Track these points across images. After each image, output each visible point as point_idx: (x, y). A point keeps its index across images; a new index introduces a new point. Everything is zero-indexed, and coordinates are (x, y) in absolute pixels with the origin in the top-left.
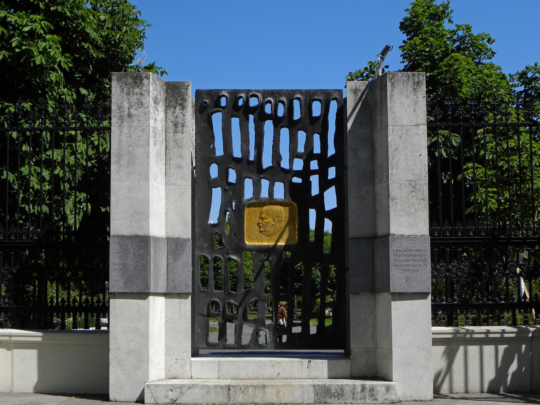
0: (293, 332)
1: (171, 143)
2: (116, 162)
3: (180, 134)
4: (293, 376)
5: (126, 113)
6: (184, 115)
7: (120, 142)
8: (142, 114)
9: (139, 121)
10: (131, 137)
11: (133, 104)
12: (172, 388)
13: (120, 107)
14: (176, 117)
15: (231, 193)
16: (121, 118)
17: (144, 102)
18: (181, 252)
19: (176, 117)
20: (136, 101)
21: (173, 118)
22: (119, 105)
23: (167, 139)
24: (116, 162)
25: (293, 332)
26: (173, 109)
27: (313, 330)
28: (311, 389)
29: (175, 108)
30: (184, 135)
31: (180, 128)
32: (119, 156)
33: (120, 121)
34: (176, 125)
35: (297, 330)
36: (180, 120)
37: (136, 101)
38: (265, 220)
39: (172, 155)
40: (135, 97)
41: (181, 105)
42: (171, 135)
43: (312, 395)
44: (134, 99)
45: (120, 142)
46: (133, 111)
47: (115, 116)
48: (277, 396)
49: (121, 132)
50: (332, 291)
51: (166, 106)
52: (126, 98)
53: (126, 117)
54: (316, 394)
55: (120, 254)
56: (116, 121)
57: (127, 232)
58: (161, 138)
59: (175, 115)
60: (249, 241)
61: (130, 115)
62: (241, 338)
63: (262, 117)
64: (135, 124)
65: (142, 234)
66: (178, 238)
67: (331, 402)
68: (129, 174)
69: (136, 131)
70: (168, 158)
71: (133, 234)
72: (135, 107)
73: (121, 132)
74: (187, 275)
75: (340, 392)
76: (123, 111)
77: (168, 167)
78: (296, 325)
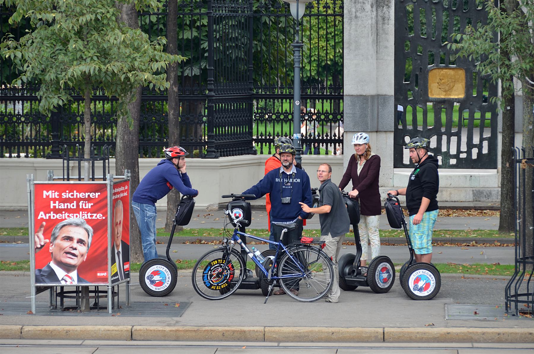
0: (461, 157)
1: (381, 31)
2: (347, 48)
3: (386, 25)
4: (460, 186)
5: (354, 15)
6: (389, 12)
7: (350, 34)
8: (364, 16)
9: (363, 21)
10: (357, 31)
11: (358, 9)
12: (384, 191)
13: (349, 11)
14: (384, 14)
15: (419, 62)
16: (351, 19)
17: (365, 8)
18: (387, 104)
19: (384, 14)
20: (360, 7)
21: (381, 14)
22: (349, 10)
23: (378, 28)
24: (347, 48)
25: (461, 157)
26: (382, 8)
27: (474, 156)
28: (471, 193)
29: (383, 7)
30: (390, 25)
31: (386, 21)
32: (350, 44)
33: (350, 21)
34: (384, 19)
35: (463, 156)
36: (386, 15)
37: (360, 7)
38: (443, 81)
39: (381, 39)
40: (359, 5)
41: (387, 5)
42: (381, 26)
43: (471, 196)
44: (359, 6)
45: (350, 34)
46: (358, 14)
47: (346, 18)
48: (450, 196)
49: (350, 28)
50: (281, 239)
51: (377, 6)
52: (353, 5)
53: (353, 18)
54: (474, 195)
55: (351, 107)
56: (347, 21)
57: (355, 93)
58: (370, 22)
59: (383, 12)
60: (431, 95)
61: (356, 17)
62: (177, 279)
63: (456, 156)
64: (360, 23)
65: (364, 94)
66: (385, 95)
67: (483, 200)
68: (356, 55)
69: (360, 27)
70: (378, 41)
71: (358, 94)
72: (360, 12)
73: (350, 28)
74: (391, 119)
75: (489, 194)
76: (352, 14)
77: (378, 48)
78: (462, 152)
